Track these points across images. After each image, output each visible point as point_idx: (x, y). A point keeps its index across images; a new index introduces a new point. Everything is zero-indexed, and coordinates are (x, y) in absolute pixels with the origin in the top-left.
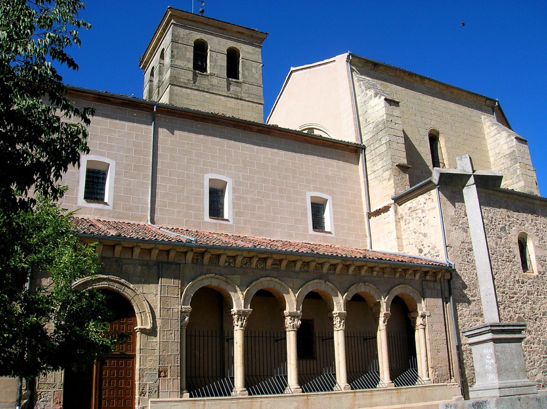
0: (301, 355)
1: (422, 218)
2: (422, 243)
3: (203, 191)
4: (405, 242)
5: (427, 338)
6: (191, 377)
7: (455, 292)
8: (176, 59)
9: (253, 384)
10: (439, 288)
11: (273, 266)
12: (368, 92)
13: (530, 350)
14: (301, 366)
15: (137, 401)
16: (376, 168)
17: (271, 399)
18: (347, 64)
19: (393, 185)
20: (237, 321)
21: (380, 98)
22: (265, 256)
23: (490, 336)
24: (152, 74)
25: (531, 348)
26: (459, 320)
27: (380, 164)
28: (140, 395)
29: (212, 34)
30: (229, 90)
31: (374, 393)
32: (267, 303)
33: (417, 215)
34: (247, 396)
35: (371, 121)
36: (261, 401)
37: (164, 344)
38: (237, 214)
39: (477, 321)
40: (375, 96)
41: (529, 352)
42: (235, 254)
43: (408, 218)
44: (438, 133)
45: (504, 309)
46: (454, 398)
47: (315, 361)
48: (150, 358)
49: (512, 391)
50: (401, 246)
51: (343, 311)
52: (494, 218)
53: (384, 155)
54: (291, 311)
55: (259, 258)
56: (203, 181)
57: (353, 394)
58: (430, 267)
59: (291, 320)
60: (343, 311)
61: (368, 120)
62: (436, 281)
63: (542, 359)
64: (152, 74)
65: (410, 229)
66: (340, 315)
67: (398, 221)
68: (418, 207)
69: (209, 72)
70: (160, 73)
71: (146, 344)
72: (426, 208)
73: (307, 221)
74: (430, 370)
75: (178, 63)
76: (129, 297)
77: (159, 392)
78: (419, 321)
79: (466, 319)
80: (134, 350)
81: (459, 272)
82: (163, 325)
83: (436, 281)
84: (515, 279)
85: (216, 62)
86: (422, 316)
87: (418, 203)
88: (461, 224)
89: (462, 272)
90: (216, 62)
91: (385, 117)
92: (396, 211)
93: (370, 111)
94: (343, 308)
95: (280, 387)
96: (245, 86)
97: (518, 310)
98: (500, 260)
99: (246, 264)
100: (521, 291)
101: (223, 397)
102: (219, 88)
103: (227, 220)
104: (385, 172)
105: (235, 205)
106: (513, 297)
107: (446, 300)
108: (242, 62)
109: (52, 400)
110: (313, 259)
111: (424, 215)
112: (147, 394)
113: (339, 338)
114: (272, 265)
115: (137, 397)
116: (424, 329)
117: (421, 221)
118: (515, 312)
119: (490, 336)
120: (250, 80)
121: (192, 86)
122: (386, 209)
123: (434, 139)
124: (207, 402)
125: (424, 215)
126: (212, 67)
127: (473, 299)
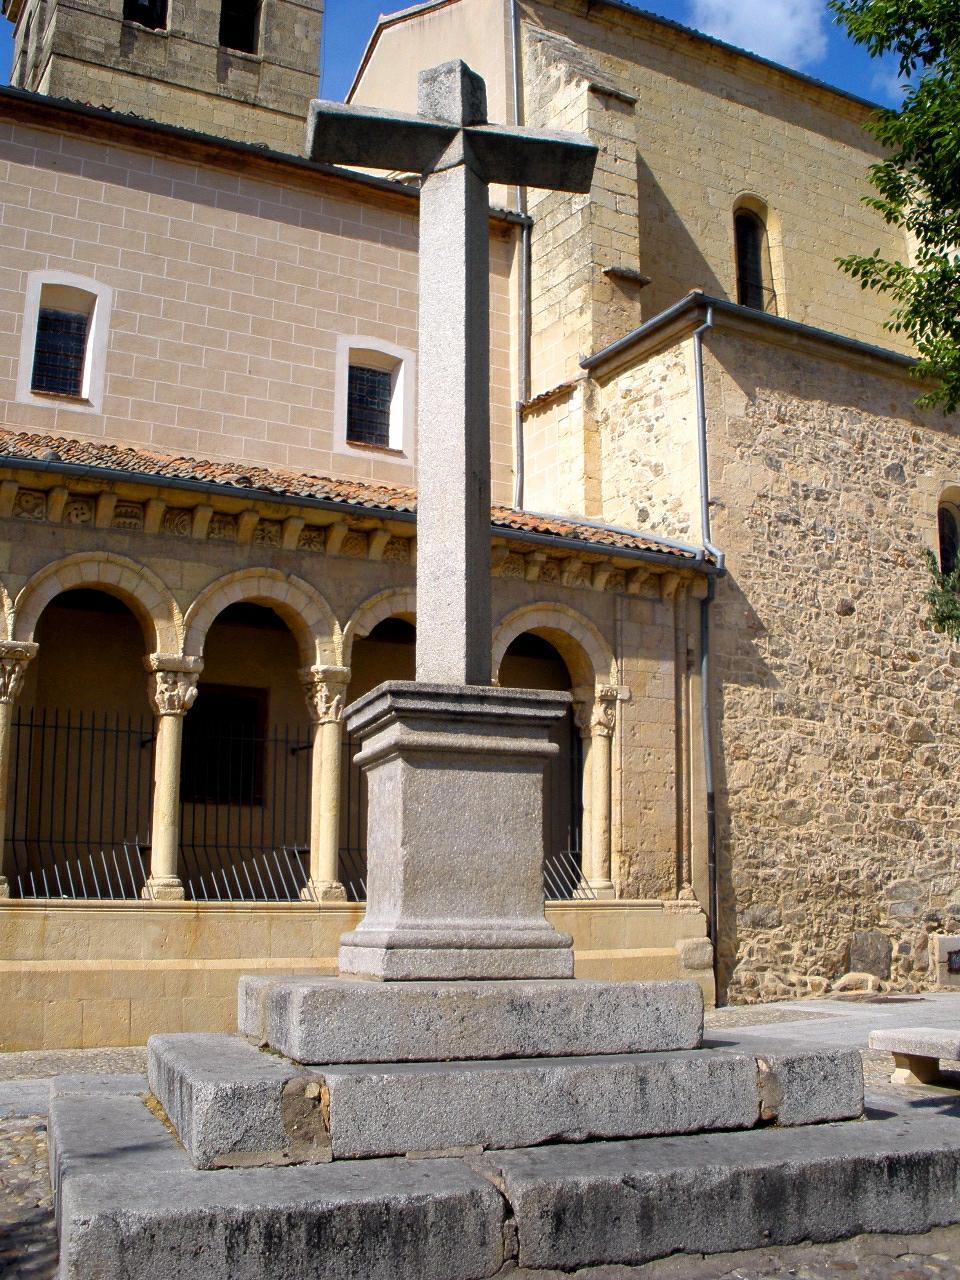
0: (189, 791)
1: (653, 422)
2: (649, 494)
3: (21, 317)
4: (607, 490)
5: (615, 764)
6: (228, 847)
7: (720, 640)
9: (200, 872)
10: (670, 622)
11: (122, 520)
13: (939, 820)
14: (188, 822)
16: (553, 280)
17: (77, 912)
19: (590, 328)
21: (578, 85)
22: (90, 488)
24: (27, 36)
25: (945, 815)
26: (725, 720)
27: (563, 269)
33: (643, 413)
34: (6, 900)
36: (46, 917)
38: (117, 385)
39: (783, 726)
40: (568, 82)
41: (937, 826)
43: (619, 420)
44: (764, 207)
45: (873, 698)
46: (681, 945)
47: (257, 811)
50: (594, 500)
51: (339, 666)
52: (871, 437)
53: (575, 243)
54: (167, 656)
56: (24, 287)
57: (348, 914)
58: (639, 558)
59: (165, 682)
60: (339, 666)
62: (661, 600)
64: (27, 36)
65: (623, 452)
66: (328, 676)
67: (592, 429)
68: (646, 390)
69: (169, 28)
72: (666, 393)
74: (616, 859)
78: (598, 712)
79: (749, 718)
81: (739, 581)
83: (661, 600)
84: (918, 616)
86: (603, 699)
87: (649, 380)
88: (763, 444)
89: (749, 582)
92: (590, 401)
94: (339, 659)
96: (270, 72)
97: (915, 704)
98: (874, 558)
100: (931, 651)
104: (572, 290)
105: (111, 361)
106: (905, 668)
107: (686, 665)
111: (658, 411)
116: (609, 738)
117: (650, 429)
118: (907, 711)
121: (117, 63)
122: (564, 393)
123: (748, 225)
125: (658, 411)
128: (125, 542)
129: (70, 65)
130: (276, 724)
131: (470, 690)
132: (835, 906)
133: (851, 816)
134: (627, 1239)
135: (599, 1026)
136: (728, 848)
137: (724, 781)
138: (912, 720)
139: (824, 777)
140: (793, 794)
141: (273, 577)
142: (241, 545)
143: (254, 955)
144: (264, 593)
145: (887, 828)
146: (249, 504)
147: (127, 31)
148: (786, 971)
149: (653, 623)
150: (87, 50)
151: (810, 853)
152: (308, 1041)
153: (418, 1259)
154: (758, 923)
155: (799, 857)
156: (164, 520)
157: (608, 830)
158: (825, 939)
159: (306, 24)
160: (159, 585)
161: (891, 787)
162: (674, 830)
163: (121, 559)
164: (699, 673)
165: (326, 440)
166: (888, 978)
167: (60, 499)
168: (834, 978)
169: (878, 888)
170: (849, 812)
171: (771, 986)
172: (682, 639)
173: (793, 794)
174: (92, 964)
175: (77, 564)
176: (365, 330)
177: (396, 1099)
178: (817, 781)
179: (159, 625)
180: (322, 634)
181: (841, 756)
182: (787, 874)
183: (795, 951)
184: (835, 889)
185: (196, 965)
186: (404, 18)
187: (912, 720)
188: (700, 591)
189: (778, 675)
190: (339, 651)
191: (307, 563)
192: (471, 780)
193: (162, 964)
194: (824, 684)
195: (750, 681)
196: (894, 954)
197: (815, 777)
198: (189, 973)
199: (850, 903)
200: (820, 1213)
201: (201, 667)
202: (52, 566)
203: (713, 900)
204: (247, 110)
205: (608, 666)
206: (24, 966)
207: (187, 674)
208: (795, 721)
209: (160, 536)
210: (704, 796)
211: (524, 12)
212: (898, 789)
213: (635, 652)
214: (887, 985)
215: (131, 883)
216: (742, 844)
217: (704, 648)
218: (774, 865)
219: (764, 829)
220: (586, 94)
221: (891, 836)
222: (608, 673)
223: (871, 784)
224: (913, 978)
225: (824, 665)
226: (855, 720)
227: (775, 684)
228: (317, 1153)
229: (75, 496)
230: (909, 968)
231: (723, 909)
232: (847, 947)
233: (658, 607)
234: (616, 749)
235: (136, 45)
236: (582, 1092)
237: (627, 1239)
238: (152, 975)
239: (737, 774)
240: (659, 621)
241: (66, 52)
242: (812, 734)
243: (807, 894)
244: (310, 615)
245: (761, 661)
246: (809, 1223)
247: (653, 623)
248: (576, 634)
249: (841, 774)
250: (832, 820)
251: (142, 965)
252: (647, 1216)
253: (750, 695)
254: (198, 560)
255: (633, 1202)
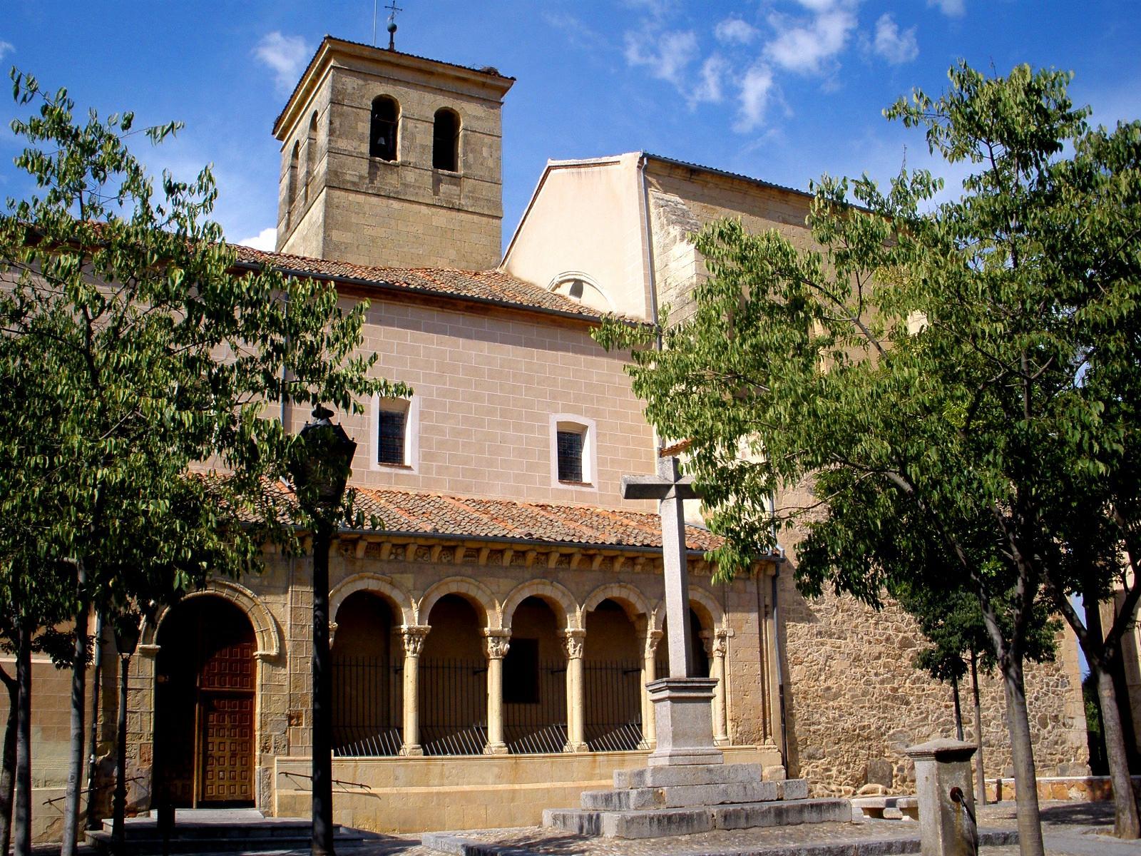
0: (508, 696)
3: (369, 419)
8: (339, 136)
9: (429, 739)
10: (755, 591)
12: (671, 228)
15: (257, 760)
17: (458, 762)
18: (638, 172)
20: (409, 643)
23: (666, 693)
25: (924, 690)
28: (262, 751)
29: (407, 84)
30: (436, 192)
31: (627, 758)
32: (456, 617)
35: (673, 285)
37: (296, 679)
38: (427, 456)
39: (822, 644)
41: (919, 697)
42: (405, 542)
45: (876, 624)
48: (276, 698)
49: (686, 760)
51: (580, 629)
54: (494, 629)
55: (443, 547)
57: (590, 758)
61: (669, 281)
62: (749, 579)
63: (943, 709)
66: (575, 634)
70: (311, 158)
71: (270, 677)
73: (548, 466)
74: (729, 724)
75: (342, 144)
76: (244, 608)
77: (289, 747)
78: (716, 644)
79: (802, 641)
80: (253, 686)
82: (294, 652)
83: (749, 579)
85: (413, 138)
86: (719, 637)
90: (413, 138)
91: (695, 280)
93: (672, 265)
94: (580, 625)
95: (557, 743)
96: (468, 184)
97: (903, 626)
99: (422, 557)
101: (473, 756)
102: (417, 190)
103: (409, 468)
105: (422, 441)
107: (765, 614)
108: (465, 136)
109: (138, 757)
110: (531, 547)
112: (272, 749)
113: (574, 672)
114: (465, 556)
115: (258, 753)
116: (723, 658)
118: (898, 630)
119: (666, 693)
120: (478, 171)
121: (367, 188)
124: (359, 763)
126: (406, 150)
127: (818, 607)
128: (469, 570)
129: (338, 193)
130: (544, 659)
131: (689, 679)
132: (857, 746)
133: (864, 694)
134: (742, 823)
135: (732, 776)
136: (792, 715)
137: (788, 678)
138: (901, 635)
139: (848, 672)
140: (829, 683)
141: (544, 584)
142: (527, 568)
143: (545, 781)
144: (540, 592)
145: (887, 700)
146: (531, 547)
147: (373, 165)
148: (829, 784)
149: (745, 592)
150: (348, 182)
151: (840, 716)
152: (654, 781)
153: (692, 826)
154: (811, 757)
155: (834, 718)
156: (488, 557)
157: (725, 708)
158: (852, 765)
159: (490, 147)
160: (488, 592)
161: (889, 675)
162: (761, 707)
163: (469, 580)
164: (772, 618)
165: (546, 480)
166: (891, 786)
167: (438, 550)
168: (858, 787)
169: (883, 734)
170: (864, 692)
171: (821, 792)
172: (762, 599)
173: (829, 683)
174: (466, 788)
175: (447, 584)
176: (566, 409)
177: (681, 792)
178: (844, 675)
179: (489, 613)
180: (570, 612)
181: (857, 659)
182: (827, 729)
183: (834, 772)
184: (853, 736)
185: (517, 787)
186: (566, 167)
187: (901, 635)
188: (771, 571)
189: (818, 615)
190: (579, 621)
191: (561, 575)
192: (690, 706)
193: (500, 787)
194: (846, 618)
195: (802, 620)
196: (895, 772)
197: (842, 672)
198: (514, 791)
199: (866, 744)
200: (792, 817)
201: (511, 634)
202: (435, 585)
203: (785, 745)
204: (454, 214)
205: (721, 618)
206: (435, 789)
207: (504, 637)
208: (829, 641)
209: (487, 565)
210: (777, 687)
211: (650, 182)
212: (893, 676)
213: (736, 610)
214: (891, 791)
215: (479, 745)
216: (800, 712)
217: (774, 604)
218: (819, 723)
219: (813, 704)
220: (693, 251)
221: (890, 704)
222: (720, 621)
223: (876, 674)
224: (907, 786)
225: (846, 607)
226: (866, 638)
227: (817, 620)
228: (662, 807)
229: (445, 548)
230: (904, 780)
231: (790, 750)
232: (865, 769)
233: (748, 583)
234: (727, 663)
235: (379, 173)
236: (729, 791)
237: (742, 823)
238: (495, 792)
239: (796, 673)
240: (748, 590)
241: (335, 185)
242: (839, 647)
243: (839, 739)
244: (564, 602)
245: (808, 608)
246: (790, 820)
247: (745, 592)
248: (703, 602)
249: (857, 670)
250: (853, 697)
251: (490, 788)
252: (747, 817)
253: (802, 628)
254: (506, 577)
255: (743, 813)
